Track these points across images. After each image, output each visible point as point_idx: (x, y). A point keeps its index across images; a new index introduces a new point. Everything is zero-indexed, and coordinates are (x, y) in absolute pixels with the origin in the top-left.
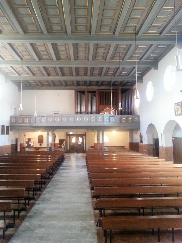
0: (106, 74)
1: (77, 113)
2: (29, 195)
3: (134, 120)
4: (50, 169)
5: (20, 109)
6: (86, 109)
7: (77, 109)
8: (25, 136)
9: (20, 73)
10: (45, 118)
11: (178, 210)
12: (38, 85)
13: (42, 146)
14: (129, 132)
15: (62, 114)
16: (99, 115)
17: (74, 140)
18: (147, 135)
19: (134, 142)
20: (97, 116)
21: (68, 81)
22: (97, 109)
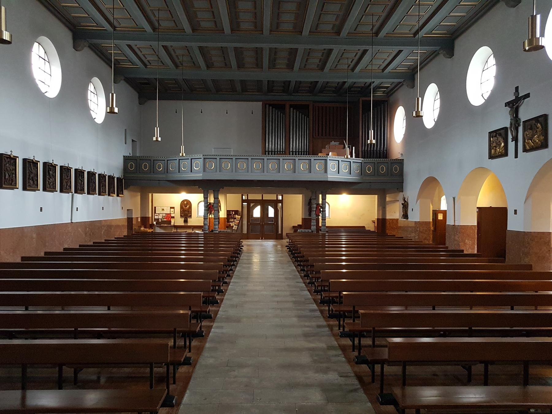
5: (154, 139)
6: (287, 144)
7: (267, 144)
9: (179, 63)
11: (469, 370)
14: (376, 196)
17: (257, 212)
20: (297, 159)
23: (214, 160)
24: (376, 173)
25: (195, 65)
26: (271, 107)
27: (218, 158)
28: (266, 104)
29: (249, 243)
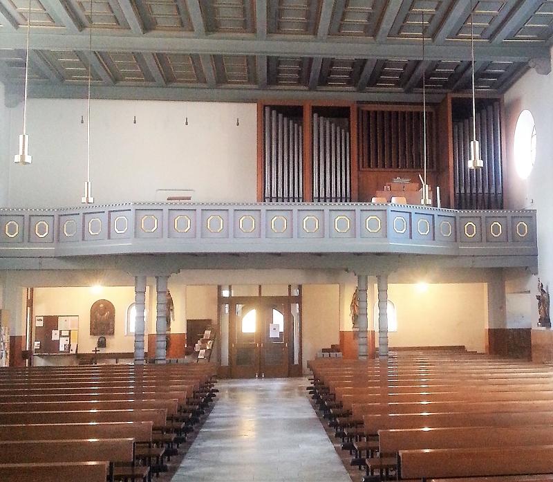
0: (398, 27)
1: (263, 198)
2: (133, 471)
3: (513, 229)
4: (137, 457)
5: (17, 158)
8: (30, 303)
9: (18, 17)
12: (96, 77)
13: (108, 351)
14: (486, 285)
15: (204, 201)
16: (363, 206)
19: (509, 327)
22: (355, 185)
23: (158, 214)
24: (484, 238)
25: (117, 22)
26: (274, 112)
27: (231, 209)
28: (265, 106)
29: (232, 385)
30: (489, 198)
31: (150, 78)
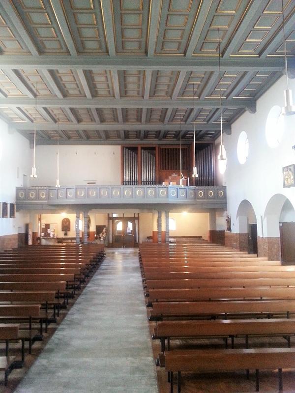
0: (171, 119)
1: (124, 183)
3: (218, 193)
4: (81, 273)
5: (32, 176)
6: (140, 176)
7: (125, 177)
8: (40, 219)
9: (33, 119)
10: (73, 191)
12: (61, 137)
13: (68, 237)
14: (208, 214)
15: (101, 185)
16: (161, 186)
17: (119, 227)
18: (238, 218)
19: (217, 230)
20: (157, 187)
21: (109, 131)
22: (158, 177)
30: (209, 182)
31: (81, 137)
